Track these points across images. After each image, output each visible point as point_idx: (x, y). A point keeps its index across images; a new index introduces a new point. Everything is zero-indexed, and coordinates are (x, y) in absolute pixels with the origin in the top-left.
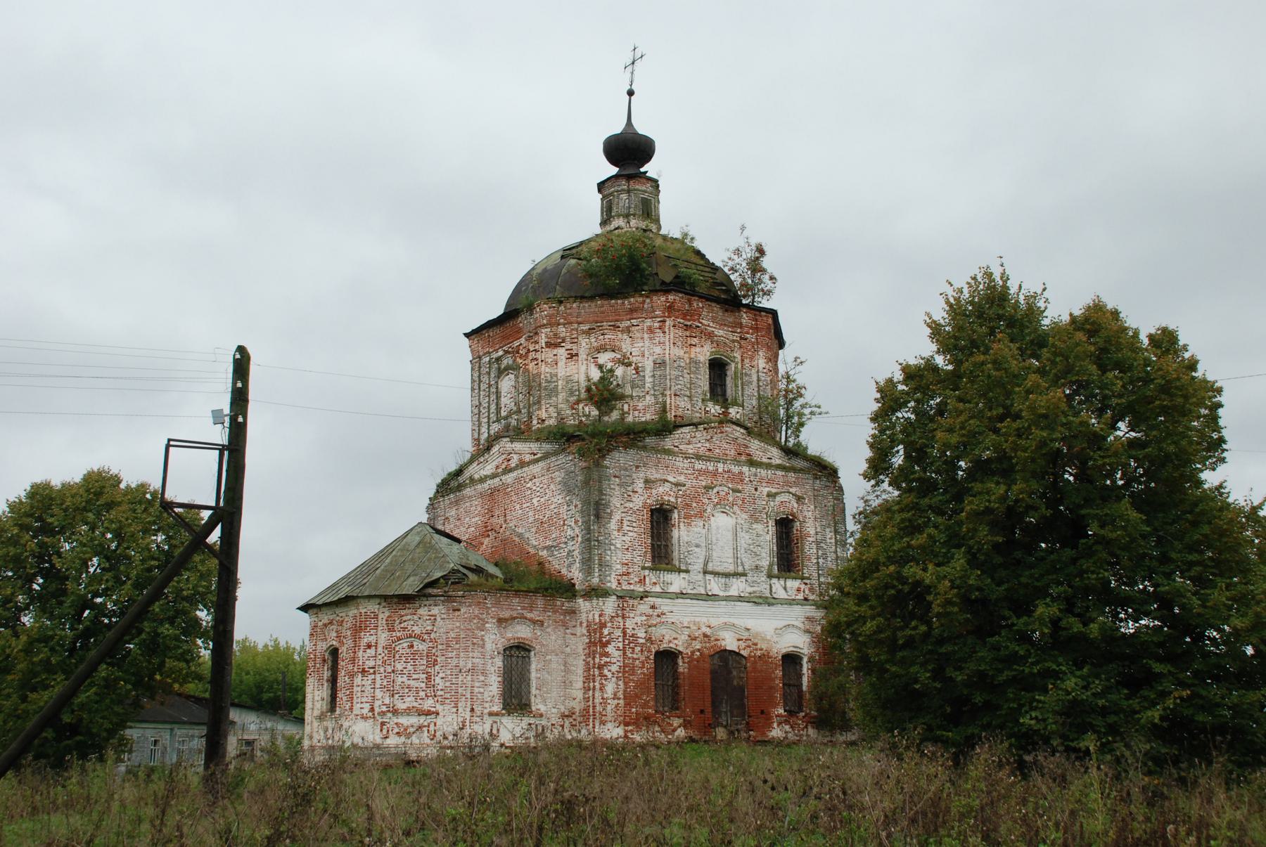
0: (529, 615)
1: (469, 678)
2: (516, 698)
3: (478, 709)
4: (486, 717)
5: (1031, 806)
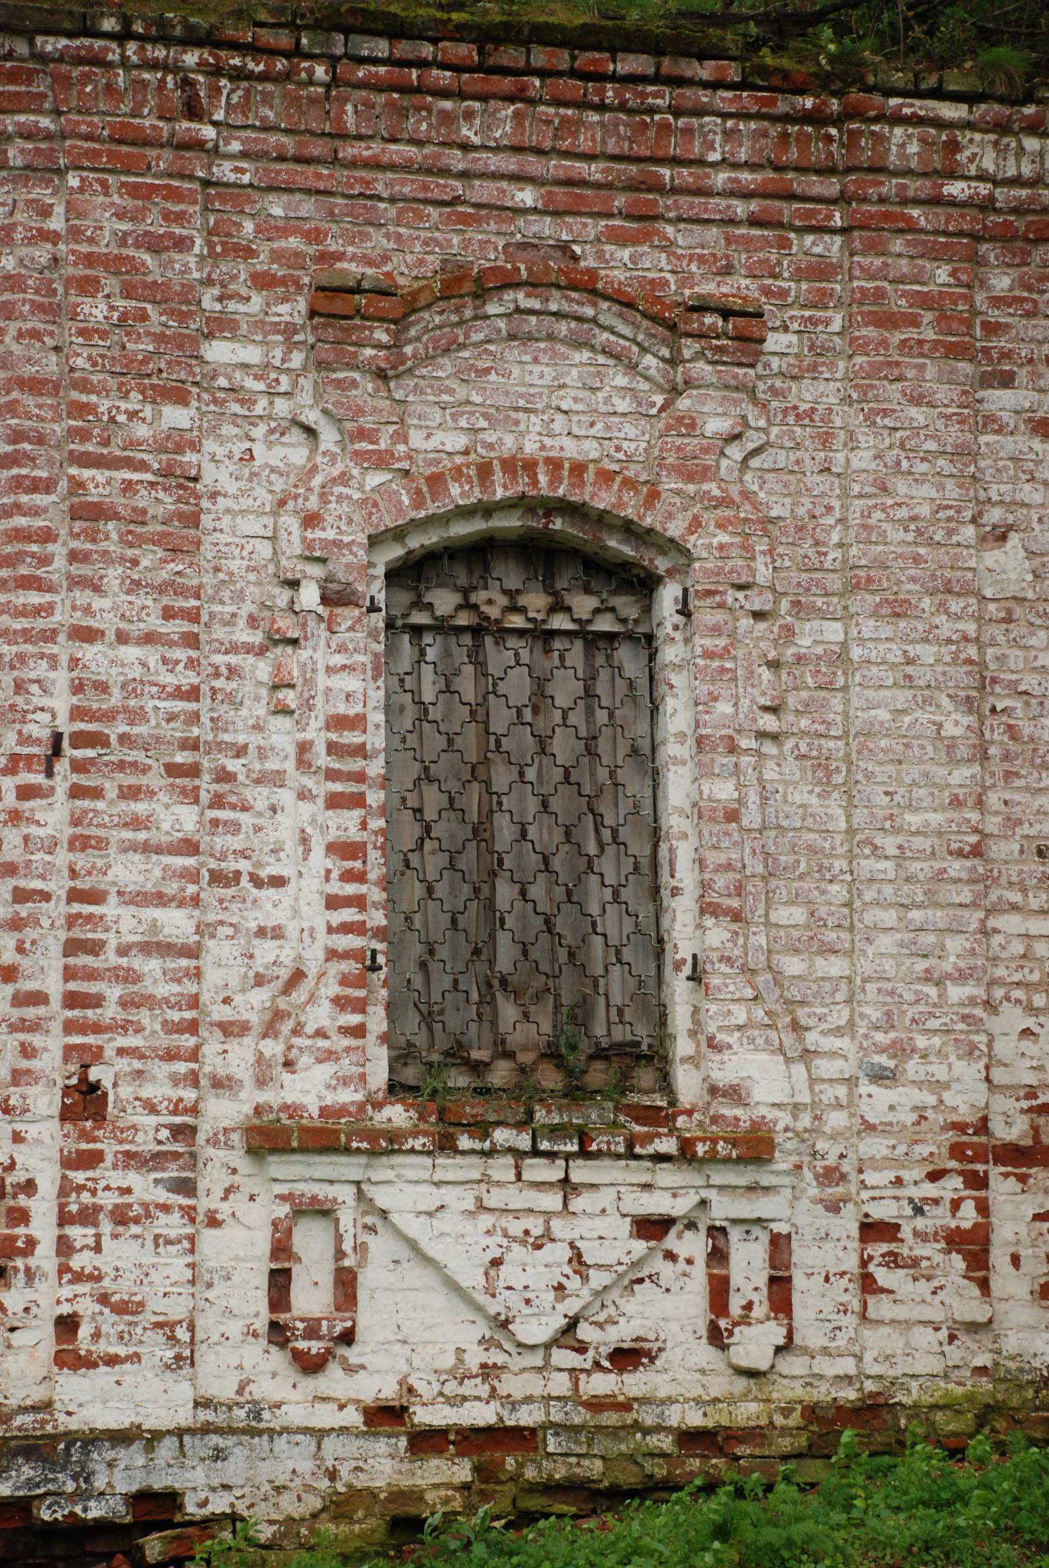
0: (621, 264)
1: (53, 816)
2: (525, 1011)
3: (141, 1096)
4: (220, 1166)
5: (930, 1190)
